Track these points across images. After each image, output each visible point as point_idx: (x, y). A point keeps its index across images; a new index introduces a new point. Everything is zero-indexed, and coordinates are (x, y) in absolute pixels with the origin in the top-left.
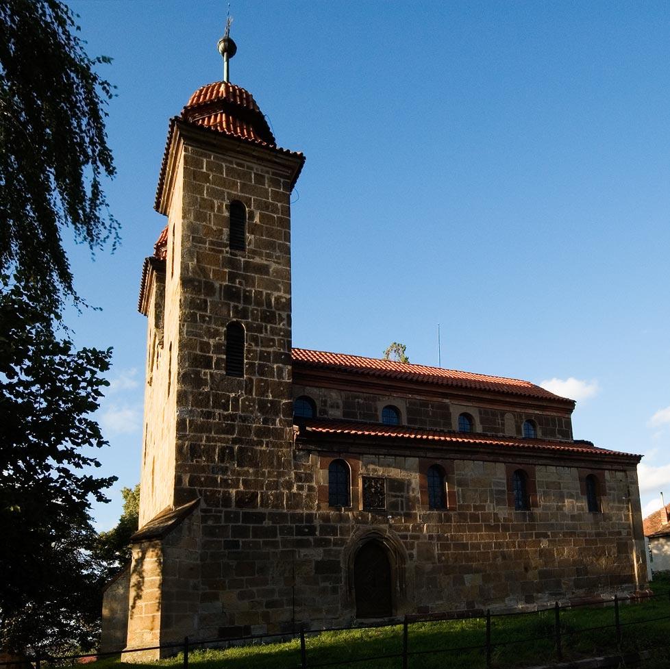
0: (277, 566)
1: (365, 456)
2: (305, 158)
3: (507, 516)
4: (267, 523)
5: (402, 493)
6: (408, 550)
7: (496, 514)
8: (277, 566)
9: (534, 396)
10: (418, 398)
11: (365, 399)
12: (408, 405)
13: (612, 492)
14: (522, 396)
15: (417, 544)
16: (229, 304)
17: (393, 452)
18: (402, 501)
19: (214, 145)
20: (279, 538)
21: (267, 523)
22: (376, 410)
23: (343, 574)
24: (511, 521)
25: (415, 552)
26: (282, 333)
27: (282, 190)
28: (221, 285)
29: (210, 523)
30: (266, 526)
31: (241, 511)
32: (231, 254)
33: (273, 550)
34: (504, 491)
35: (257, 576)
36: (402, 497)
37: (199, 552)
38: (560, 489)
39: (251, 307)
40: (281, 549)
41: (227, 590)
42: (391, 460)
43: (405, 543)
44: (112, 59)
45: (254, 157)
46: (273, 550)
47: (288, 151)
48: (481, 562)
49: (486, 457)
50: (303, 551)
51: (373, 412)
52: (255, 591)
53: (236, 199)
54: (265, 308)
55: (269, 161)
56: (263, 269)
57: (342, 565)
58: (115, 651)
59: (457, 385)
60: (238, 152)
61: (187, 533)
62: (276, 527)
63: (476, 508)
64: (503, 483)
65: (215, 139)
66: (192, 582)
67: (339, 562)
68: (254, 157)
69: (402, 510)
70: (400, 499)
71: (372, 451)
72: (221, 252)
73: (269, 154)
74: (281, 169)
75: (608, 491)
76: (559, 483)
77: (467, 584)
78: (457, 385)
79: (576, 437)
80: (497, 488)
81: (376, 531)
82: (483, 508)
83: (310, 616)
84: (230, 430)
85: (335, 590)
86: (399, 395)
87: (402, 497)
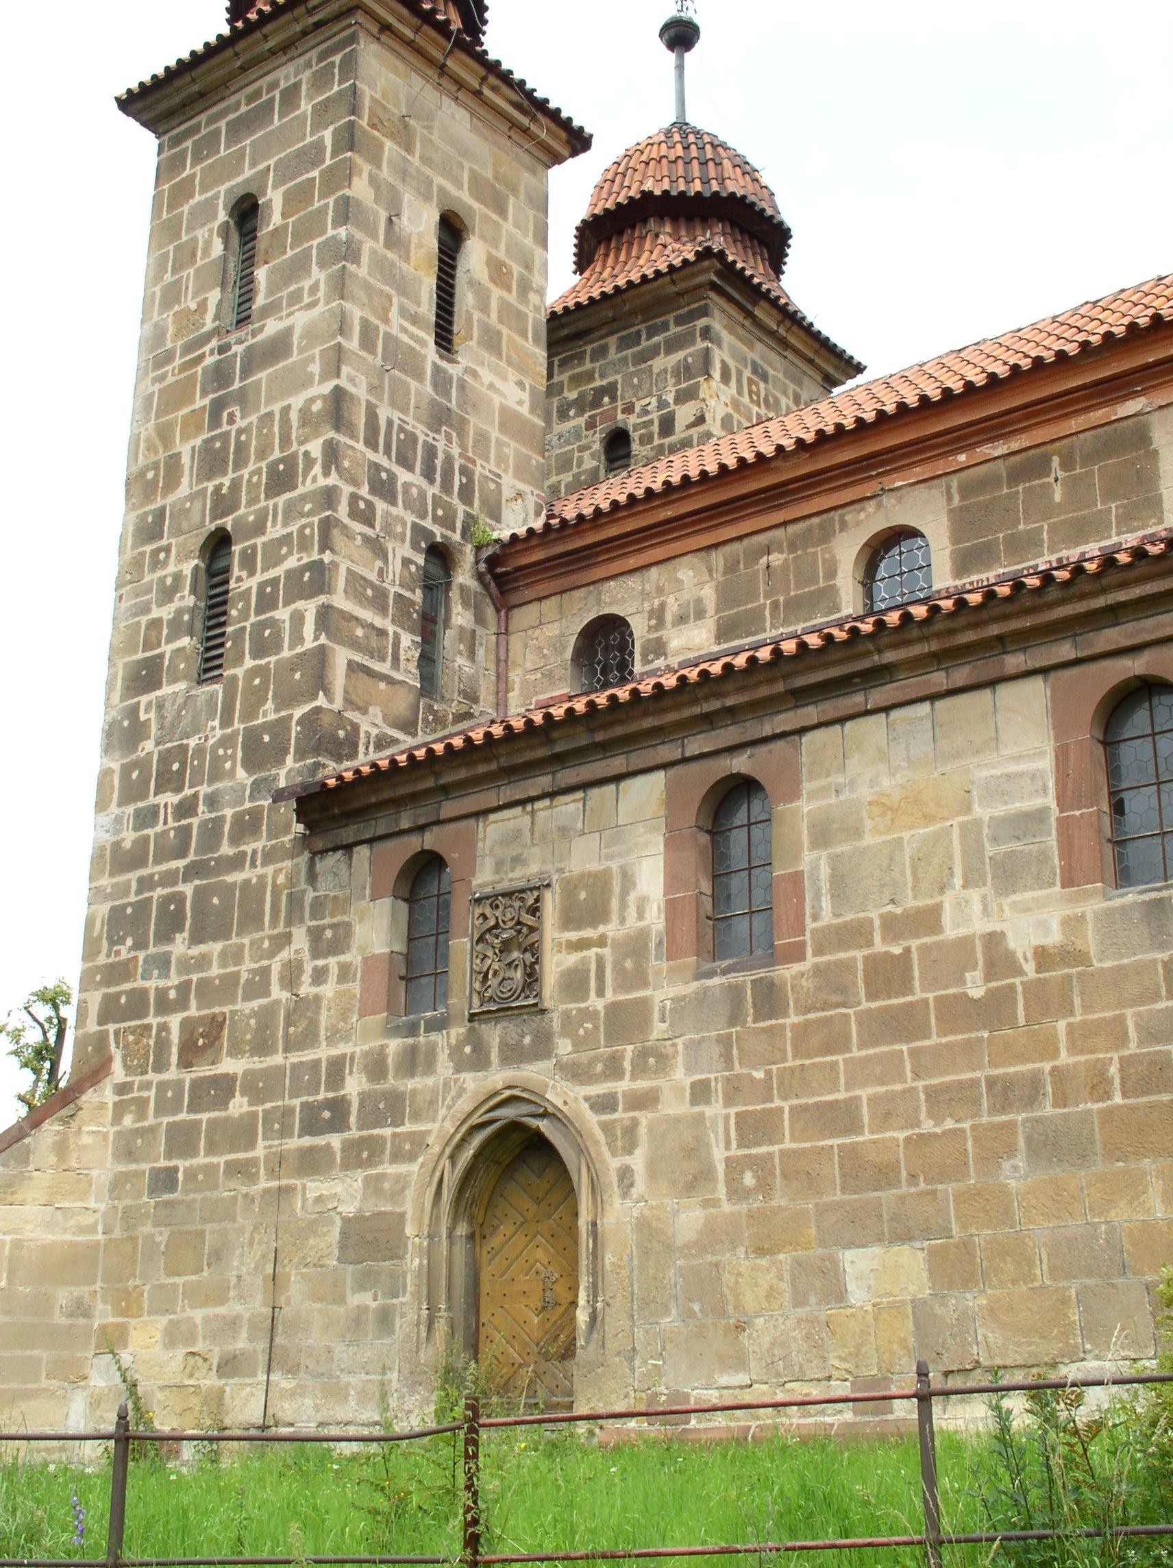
0: (251, 1243)
1: (492, 817)
5: (602, 929)
6: (614, 1155)
7: (994, 940)
8: (251, 1243)
9: (1132, 327)
10: (1000, 449)
11: (793, 547)
12: (956, 498)
14: (659, 496)
15: (650, 1129)
17: (568, 776)
19: (201, 95)
20: (260, 1150)
21: (239, 1105)
23: (413, 1262)
25: (637, 1161)
26: (308, 507)
29: (128, 1121)
31: (920, 1084)
33: (244, 1190)
34: (1039, 816)
36: (601, 942)
37: (102, 1207)
40: (264, 1183)
41: (145, 1318)
42: (572, 807)
43: (606, 1127)
45: (273, 53)
46: (244, 1190)
48: (922, 1186)
49: (939, 679)
50: (315, 1187)
52: (198, 1321)
55: (304, 33)
57: (409, 1230)
59: (881, 414)
60: (244, 69)
61: (53, 1159)
62: (254, 1115)
63: (893, 927)
65: (194, 80)
66: (63, 1296)
67: (402, 1216)
68: (273, 53)
69: (601, 992)
70: (592, 952)
71: (509, 793)
73: (296, 20)
74: (336, 29)
77: (857, 1295)
78: (881, 414)
80: (1000, 810)
81: (516, 1092)
82: (929, 920)
83: (317, 1409)
85: (385, 1319)
86: (919, 472)
87: (601, 942)
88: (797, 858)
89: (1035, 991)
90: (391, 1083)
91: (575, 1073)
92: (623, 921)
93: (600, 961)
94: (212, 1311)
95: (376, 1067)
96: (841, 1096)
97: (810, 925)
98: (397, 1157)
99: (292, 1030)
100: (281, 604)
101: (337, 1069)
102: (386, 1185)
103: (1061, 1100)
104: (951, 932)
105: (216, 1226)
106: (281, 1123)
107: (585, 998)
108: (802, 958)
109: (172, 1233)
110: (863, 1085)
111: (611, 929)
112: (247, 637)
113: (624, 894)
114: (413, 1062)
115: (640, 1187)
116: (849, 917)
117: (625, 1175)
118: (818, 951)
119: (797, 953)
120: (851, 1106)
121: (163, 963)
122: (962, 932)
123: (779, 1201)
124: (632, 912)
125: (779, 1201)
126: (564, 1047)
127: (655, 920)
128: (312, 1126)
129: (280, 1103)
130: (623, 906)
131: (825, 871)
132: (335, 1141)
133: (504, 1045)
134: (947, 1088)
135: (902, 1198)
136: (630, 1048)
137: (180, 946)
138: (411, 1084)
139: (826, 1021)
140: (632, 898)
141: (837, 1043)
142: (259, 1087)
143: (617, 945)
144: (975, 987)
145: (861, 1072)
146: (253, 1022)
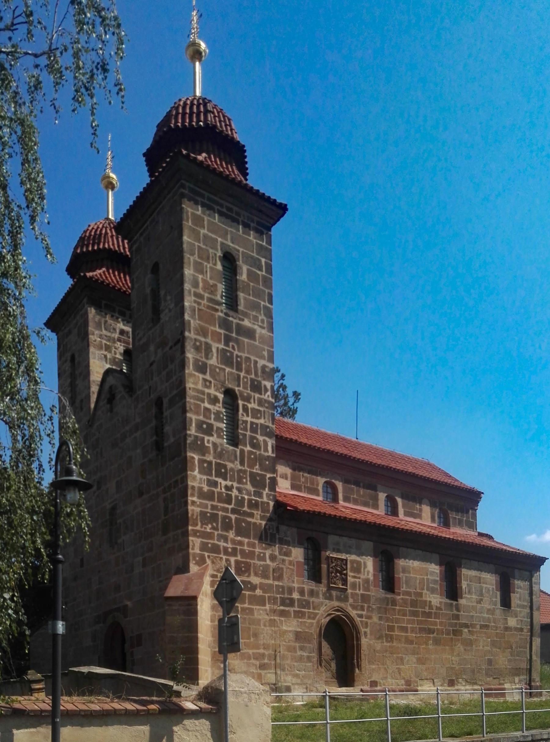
2: (287, 209)
3: (438, 605)
4: (258, 592)
13: (519, 590)
16: (225, 370)
18: (359, 582)
21: (258, 592)
22: (318, 485)
24: (441, 609)
25: (368, 630)
27: (264, 244)
28: (218, 348)
30: (258, 594)
32: (226, 314)
35: (252, 639)
36: (359, 578)
38: (480, 583)
39: (242, 374)
44: (483, 493)
47: (246, 163)
51: (315, 487)
53: (228, 250)
54: (253, 376)
56: (250, 334)
58: (323, 651)
64: (437, 573)
69: (359, 590)
72: (217, 310)
75: (516, 589)
76: (480, 577)
79: (481, 528)
84: (228, 499)
88: (399, 574)
89: (435, 613)
90: (306, 597)
91: (354, 607)
92: (364, 575)
93: (359, 582)
94: (255, 651)
95: (302, 592)
96: (405, 625)
97: (402, 589)
98: (309, 618)
99: (275, 574)
100: (270, 247)
101: (290, 590)
102: (307, 624)
103: (437, 634)
104: (424, 599)
105: (254, 627)
106: (273, 600)
107: (356, 590)
108: (400, 595)
109: (264, 379)
110: (409, 624)
111: (362, 576)
112: (120, 672)
113: (364, 569)
114: (312, 593)
115: (368, 636)
116: (408, 590)
117: (365, 633)
118: (403, 595)
119: (399, 594)
120: (407, 628)
121: (226, 539)
122: (426, 599)
123: (395, 644)
124: (366, 573)
125: (395, 644)
126: (351, 600)
127: (371, 577)
128: (283, 603)
129: (272, 595)
130: (364, 572)
131: (404, 579)
132: (292, 609)
133: (337, 596)
134: (422, 628)
135: (414, 647)
136: (366, 605)
137: (231, 534)
138: (311, 600)
139: (403, 610)
140: (366, 570)
141: (404, 615)
142: (265, 588)
143: (363, 580)
144: (427, 610)
145: (409, 622)
146: (261, 568)
